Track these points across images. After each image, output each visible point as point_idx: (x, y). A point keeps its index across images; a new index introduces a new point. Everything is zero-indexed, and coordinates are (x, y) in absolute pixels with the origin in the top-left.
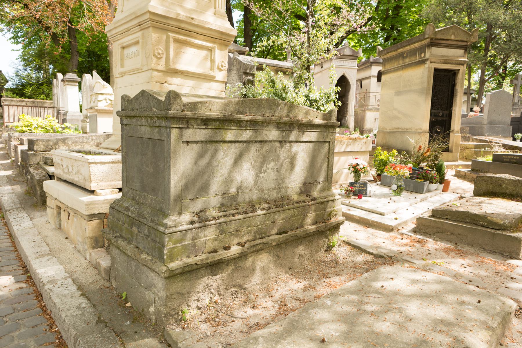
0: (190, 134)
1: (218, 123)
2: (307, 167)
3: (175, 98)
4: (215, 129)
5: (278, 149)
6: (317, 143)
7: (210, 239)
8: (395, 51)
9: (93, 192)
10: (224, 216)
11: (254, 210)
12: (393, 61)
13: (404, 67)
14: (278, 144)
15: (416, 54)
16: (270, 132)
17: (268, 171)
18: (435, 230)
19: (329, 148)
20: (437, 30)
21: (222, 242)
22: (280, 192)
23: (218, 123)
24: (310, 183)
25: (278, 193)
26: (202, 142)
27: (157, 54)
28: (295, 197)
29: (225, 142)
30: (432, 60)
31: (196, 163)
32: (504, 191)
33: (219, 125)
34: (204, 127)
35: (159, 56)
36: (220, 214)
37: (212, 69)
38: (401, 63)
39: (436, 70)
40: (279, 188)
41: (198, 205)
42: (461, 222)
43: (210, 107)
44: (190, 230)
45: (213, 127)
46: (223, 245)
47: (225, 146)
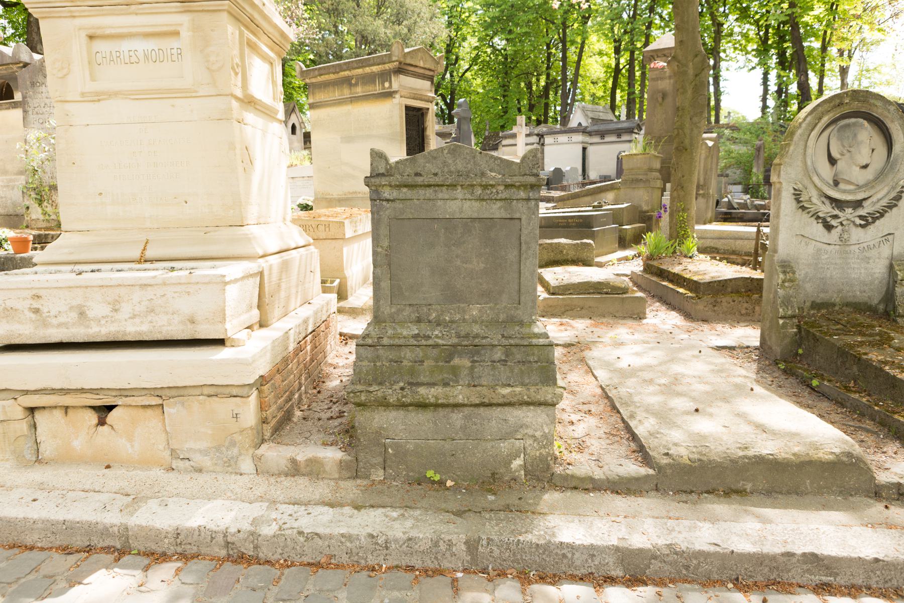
8: (334, 73)
9: (220, 342)
12: (331, 88)
13: (354, 100)
15: (374, 82)
18: (563, 309)
20: (407, 50)
30: (402, 94)
32: (565, 257)
38: (347, 92)
39: (408, 109)
42: (585, 294)
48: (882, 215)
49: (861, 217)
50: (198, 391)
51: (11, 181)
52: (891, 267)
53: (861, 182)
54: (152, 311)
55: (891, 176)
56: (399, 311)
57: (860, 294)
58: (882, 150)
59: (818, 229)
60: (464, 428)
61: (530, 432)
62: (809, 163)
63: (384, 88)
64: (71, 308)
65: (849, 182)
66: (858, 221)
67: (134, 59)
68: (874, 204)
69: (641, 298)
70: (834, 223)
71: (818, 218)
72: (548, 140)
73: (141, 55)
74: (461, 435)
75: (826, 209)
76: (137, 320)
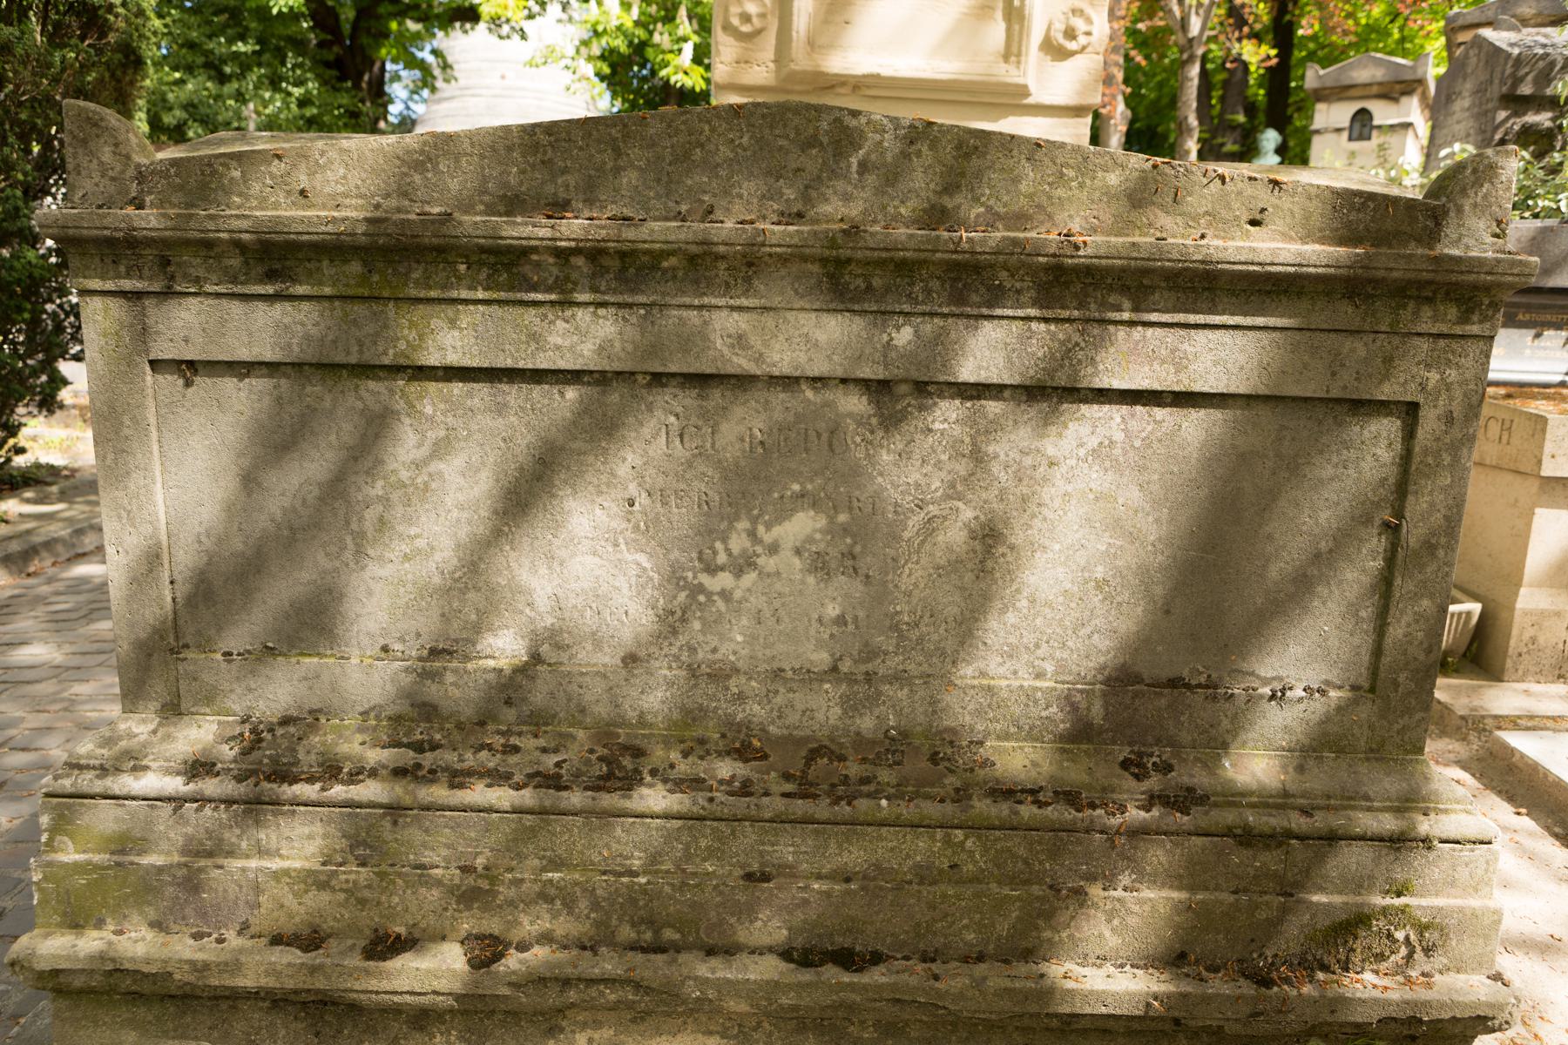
0: (187, 324)
1: (355, 267)
2: (1143, 571)
3: (84, 142)
4: (343, 298)
5: (854, 436)
6: (1264, 412)
7: (286, 872)
10: (399, 772)
11: (630, 782)
14: (854, 403)
16: (769, 320)
17: (768, 563)
19: (1406, 458)
21: (362, 902)
22: (875, 699)
23: (355, 267)
24: (1175, 683)
25: (851, 706)
26: (272, 368)
27: (735, 21)
28: (1018, 759)
29: (423, 373)
31: (250, 481)
33: (364, 280)
34: (270, 289)
35: (746, 28)
36: (374, 756)
37: (1012, 52)
40: (869, 677)
41: (277, 692)
43: (303, 181)
44: (169, 799)
45: (327, 291)
46: (370, 919)
47: (432, 399)
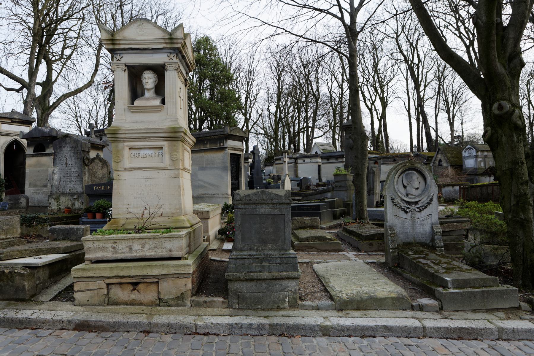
48: (426, 207)
49: (418, 208)
50: (172, 276)
51: (38, 190)
52: (432, 228)
53: (417, 194)
54: (157, 247)
55: (427, 193)
56: (244, 246)
57: (423, 240)
58: (423, 183)
59: (402, 213)
60: (266, 288)
61: (290, 289)
62: (396, 187)
63: (220, 146)
64: (127, 247)
65: (412, 195)
66: (417, 210)
67: (145, 156)
68: (422, 203)
69: (339, 243)
70: (408, 210)
71: (402, 209)
72: (300, 161)
73: (147, 154)
74: (266, 290)
75: (405, 205)
76: (151, 251)
